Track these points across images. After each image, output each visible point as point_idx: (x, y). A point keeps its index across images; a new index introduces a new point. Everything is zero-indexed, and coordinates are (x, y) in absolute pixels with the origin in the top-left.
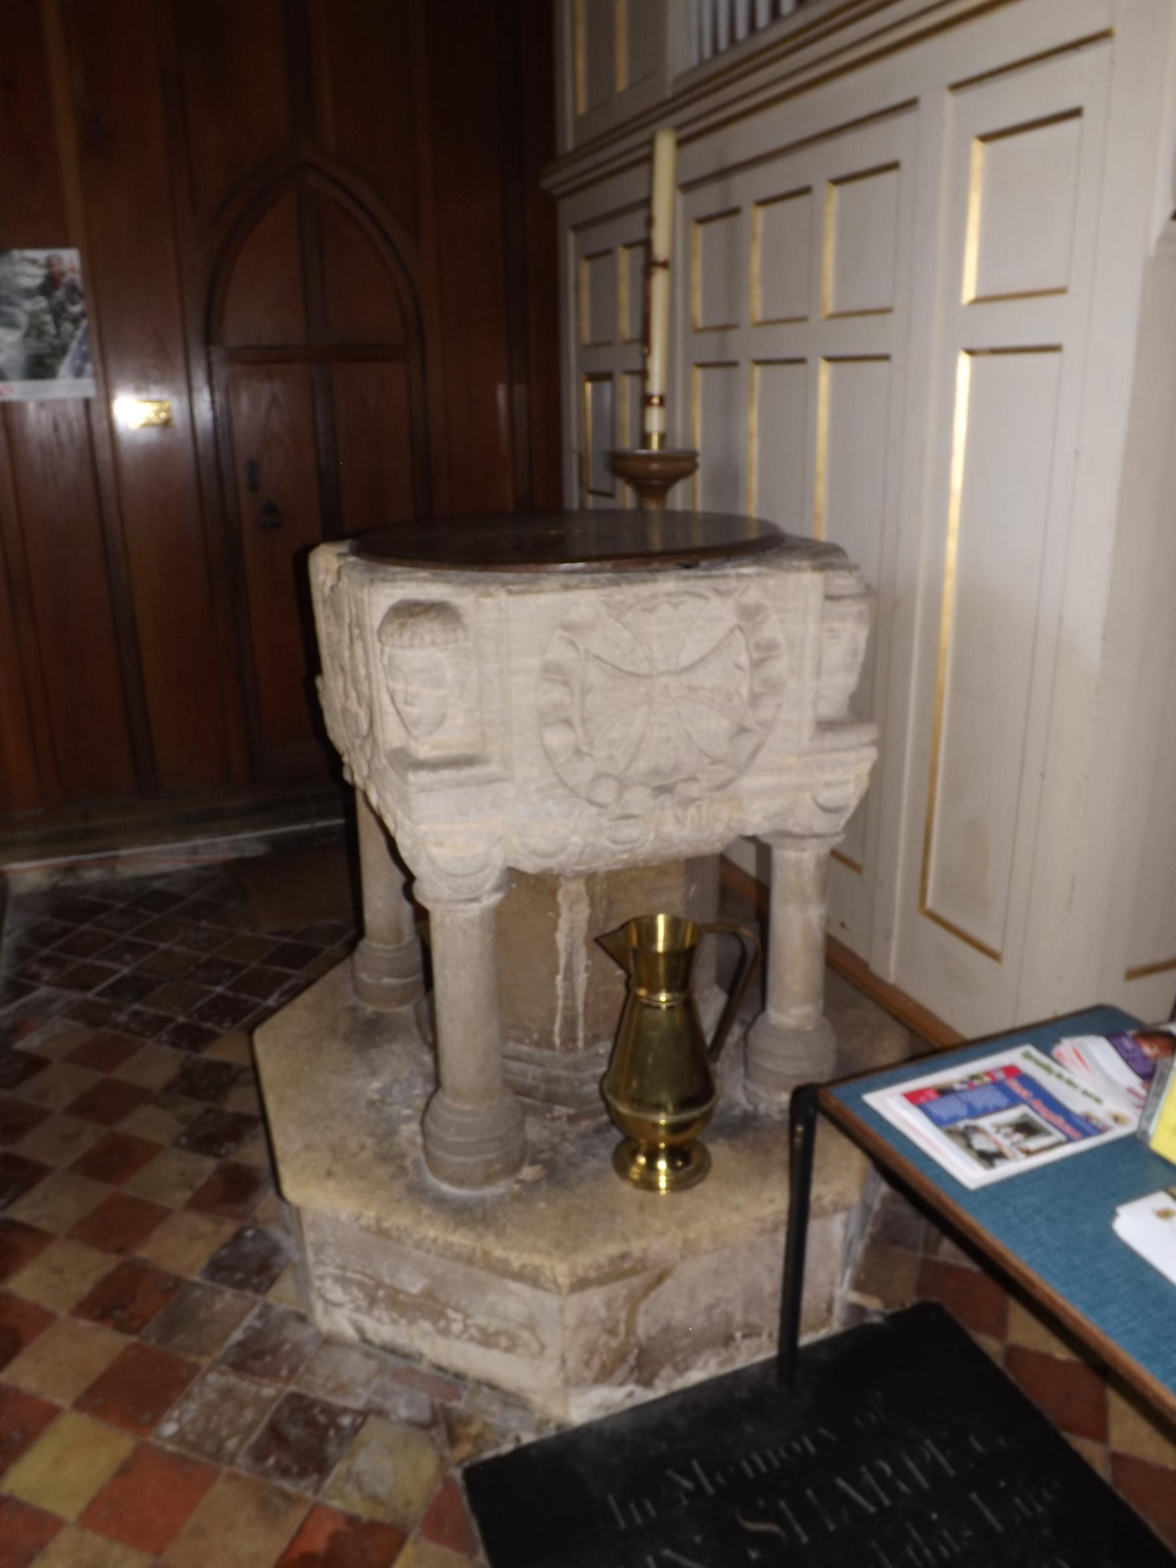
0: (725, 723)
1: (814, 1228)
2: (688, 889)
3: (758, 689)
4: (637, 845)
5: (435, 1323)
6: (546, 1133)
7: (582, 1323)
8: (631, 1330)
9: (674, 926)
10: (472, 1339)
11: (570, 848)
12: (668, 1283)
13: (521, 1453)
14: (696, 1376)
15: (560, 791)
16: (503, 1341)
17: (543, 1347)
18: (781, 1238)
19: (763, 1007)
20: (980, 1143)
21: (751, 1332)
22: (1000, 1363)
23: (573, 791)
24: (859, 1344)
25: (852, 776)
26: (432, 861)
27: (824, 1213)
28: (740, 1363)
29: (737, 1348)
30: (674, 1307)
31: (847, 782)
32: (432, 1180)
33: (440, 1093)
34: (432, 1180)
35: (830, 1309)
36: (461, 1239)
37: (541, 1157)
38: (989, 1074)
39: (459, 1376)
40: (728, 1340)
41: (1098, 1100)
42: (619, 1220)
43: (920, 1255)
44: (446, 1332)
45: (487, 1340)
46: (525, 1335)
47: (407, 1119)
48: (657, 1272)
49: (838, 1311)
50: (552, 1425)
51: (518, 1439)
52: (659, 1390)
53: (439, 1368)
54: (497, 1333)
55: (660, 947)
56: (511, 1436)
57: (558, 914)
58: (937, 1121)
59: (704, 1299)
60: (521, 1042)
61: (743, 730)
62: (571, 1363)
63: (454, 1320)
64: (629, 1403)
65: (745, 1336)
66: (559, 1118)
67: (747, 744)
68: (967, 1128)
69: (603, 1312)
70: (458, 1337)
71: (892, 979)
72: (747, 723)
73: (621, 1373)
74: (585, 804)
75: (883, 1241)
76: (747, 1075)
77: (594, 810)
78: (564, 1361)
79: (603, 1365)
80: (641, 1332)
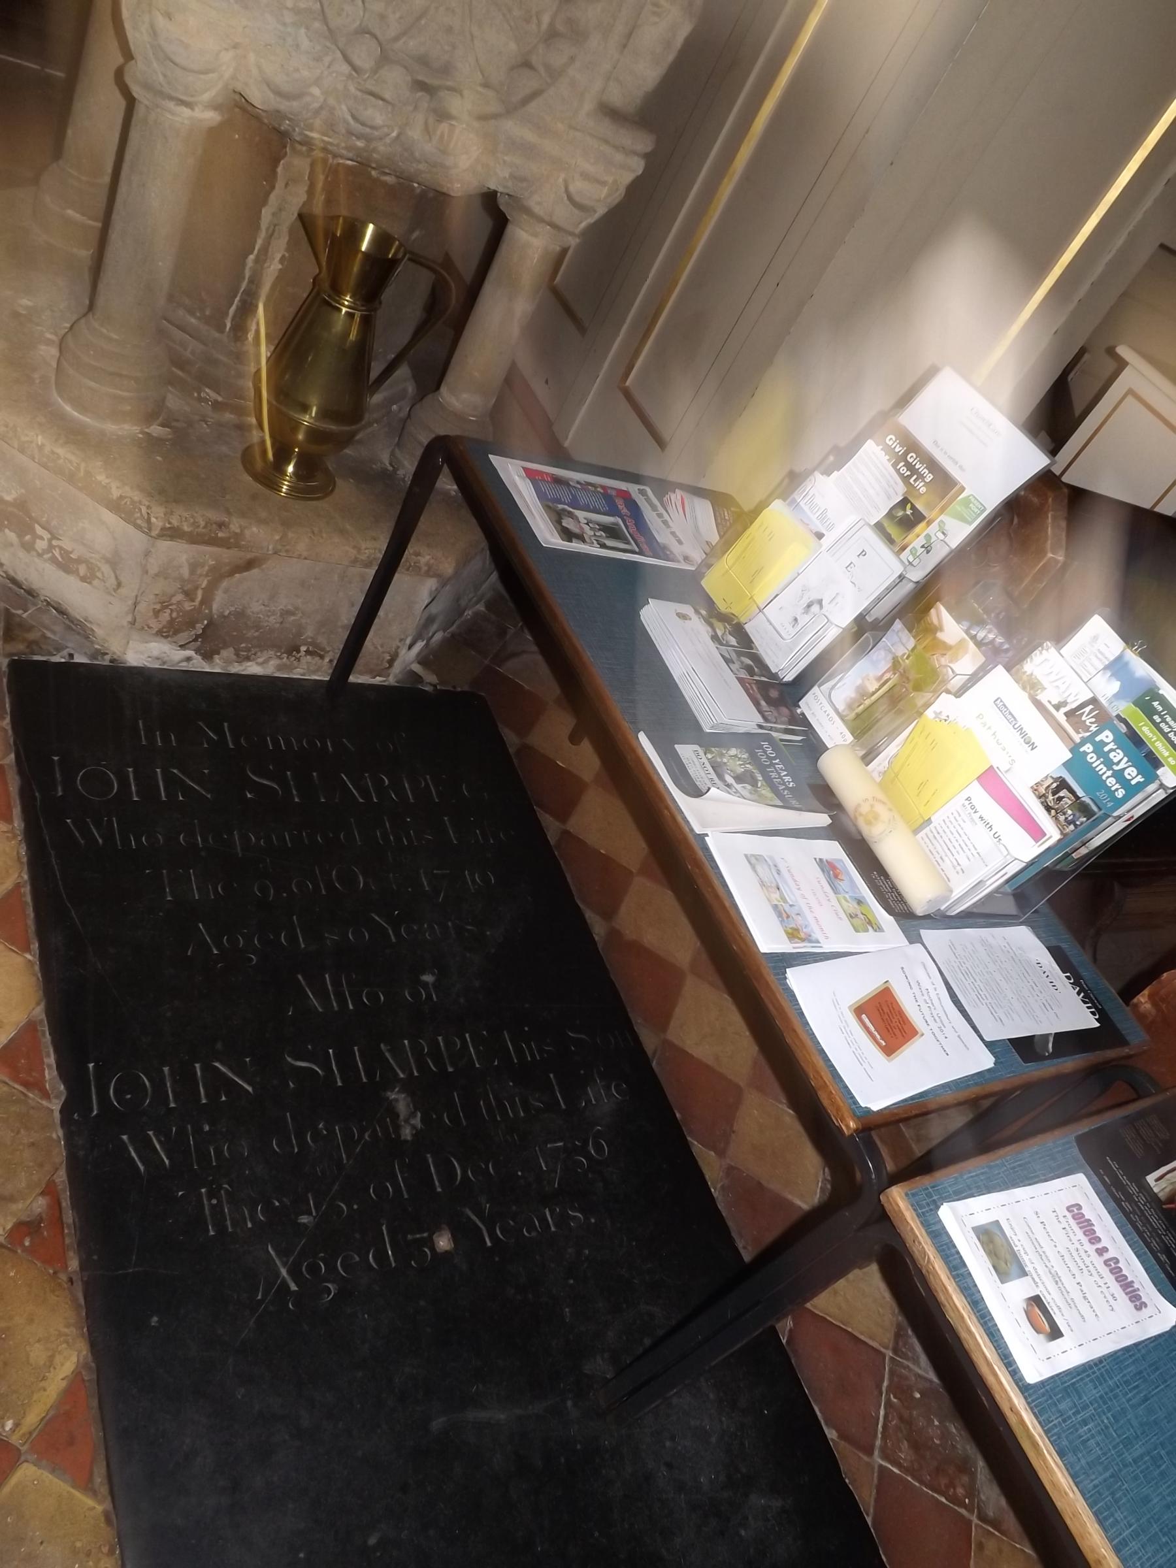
0: (513, 46)
1: (400, 580)
2: (412, 231)
3: (560, 27)
4: (376, 133)
5: (20, 536)
6: (187, 408)
7: (162, 574)
8: (207, 601)
9: (382, 240)
10: (54, 560)
11: (308, 99)
12: (255, 572)
13: (69, 669)
14: (253, 668)
15: (317, 25)
16: (82, 570)
17: (119, 585)
18: (371, 572)
19: (438, 387)
20: (567, 523)
21: (316, 652)
22: (511, 750)
23: (332, 34)
24: (402, 701)
25: (610, 179)
26: (154, 33)
27: (416, 569)
28: (296, 674)
29: (299, 660)
30: (254, 597)
31: (604, 183)
32: (56, 397)
33: (90, 315)
34: (56, 397)
35: (391, 662)
36: (66, 454)
37: (174, 424)
38: (603, 487)
39: (31, 593)
40: (293, 650)
41: (680, 542)
42: (228, 497)
43: (487, 662)
44: (28, 547)
45: (66, 564)
46: (106, 569)
47: (49, 342)
48: (249, 556)
49: (397, 668)
50: (108, 657)
51: (71, 656)
52: (216, 666)
53: (14, 581)
54: (79, 561)
55: (364, 248)
56: (65, 652)
57: (273, 188)
58: (541, 495)
59: (283, 603)
60: (192, 314)
61: (527, 65)
62: (142, 607)
63: (42, 538)
64: (184, 666)
65: (308, 652)
66: (206, 400)
67: (528, 83)
68: (564, 510)
69: (185, 572)
70: (40, 555)
71: (566, 444)
72: (534, 60)
73: (184, 637)
74: (339, 55)
75: (462, 641)
76: (398, 445)
77: (345, 68)
78: (135, 604)
79: (172, 621)
80: (215, 606)
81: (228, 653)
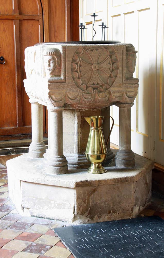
8: (88, 203)
73: (86, 214)
80: (90, 204)
81: (96, 216)
